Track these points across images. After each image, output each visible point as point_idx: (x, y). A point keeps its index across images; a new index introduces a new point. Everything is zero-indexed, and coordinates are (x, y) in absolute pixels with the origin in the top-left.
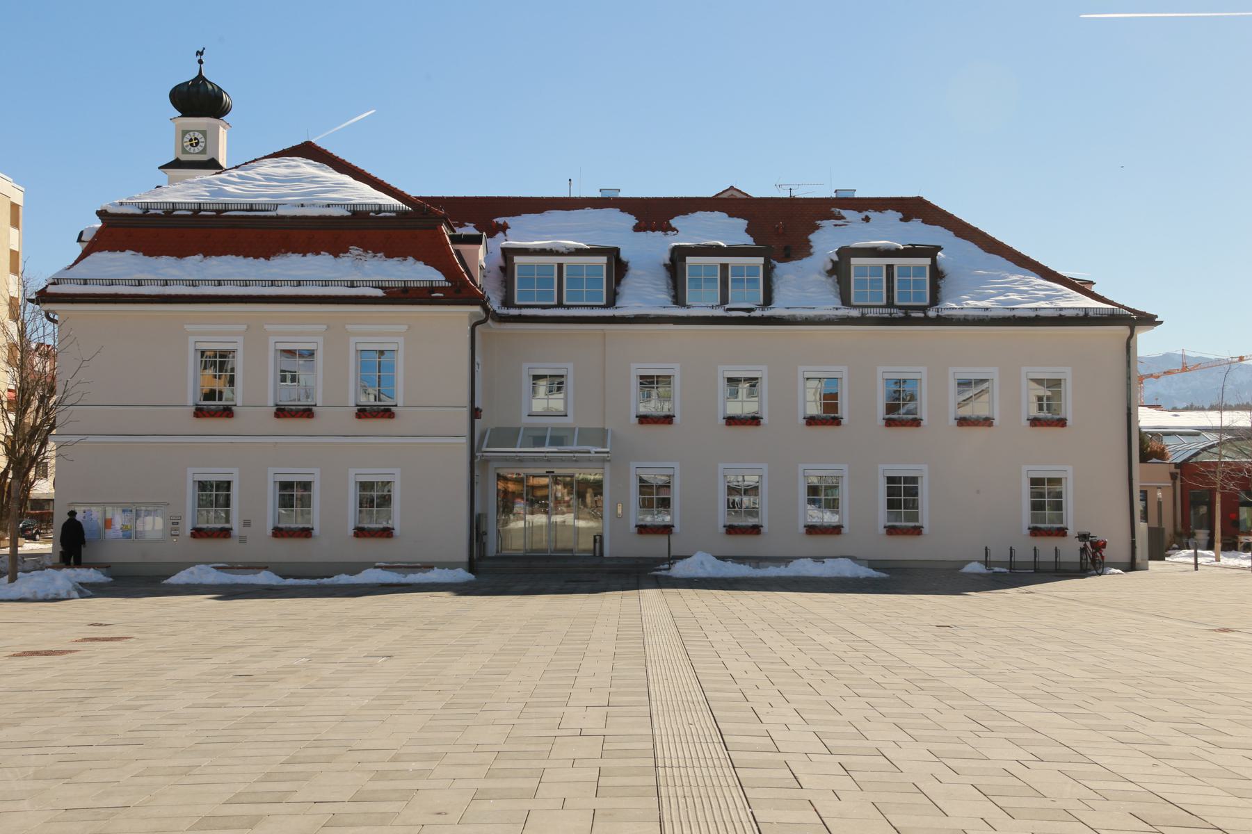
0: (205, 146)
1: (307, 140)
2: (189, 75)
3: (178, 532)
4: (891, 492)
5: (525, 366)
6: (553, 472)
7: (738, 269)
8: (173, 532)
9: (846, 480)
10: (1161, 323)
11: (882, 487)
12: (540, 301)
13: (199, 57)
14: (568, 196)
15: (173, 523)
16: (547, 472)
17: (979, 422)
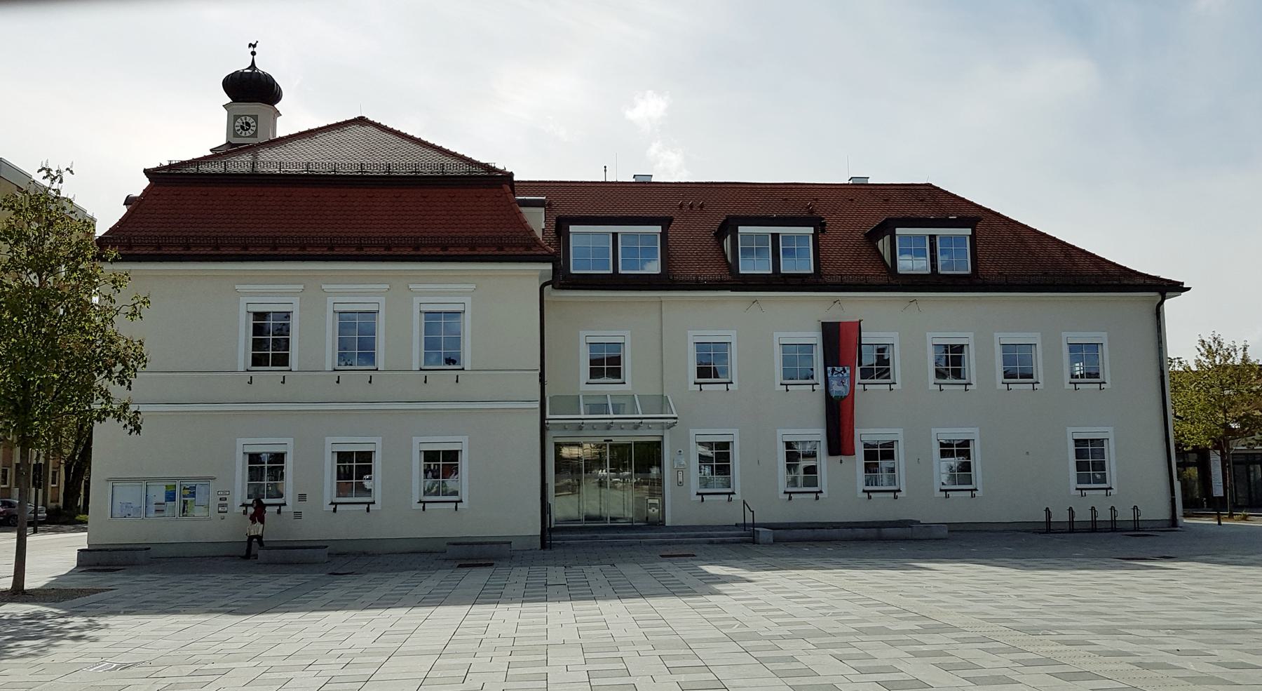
0: (256, 130)
1: (360, 115)
2: (242, 65)
3: (225, 502)
4: (1079, 454)
5: (583, 334)
6: (611, 441)
7: (788, 238)
8: (220, 509)
9: (977, 443)
10: (1189, 289)
11: (1072, 449)
12: (609, 266)
13: (251, 49)
14: (604, 180)
15: (221, 499)
16: (605, 441)
17: (1092, 376)
